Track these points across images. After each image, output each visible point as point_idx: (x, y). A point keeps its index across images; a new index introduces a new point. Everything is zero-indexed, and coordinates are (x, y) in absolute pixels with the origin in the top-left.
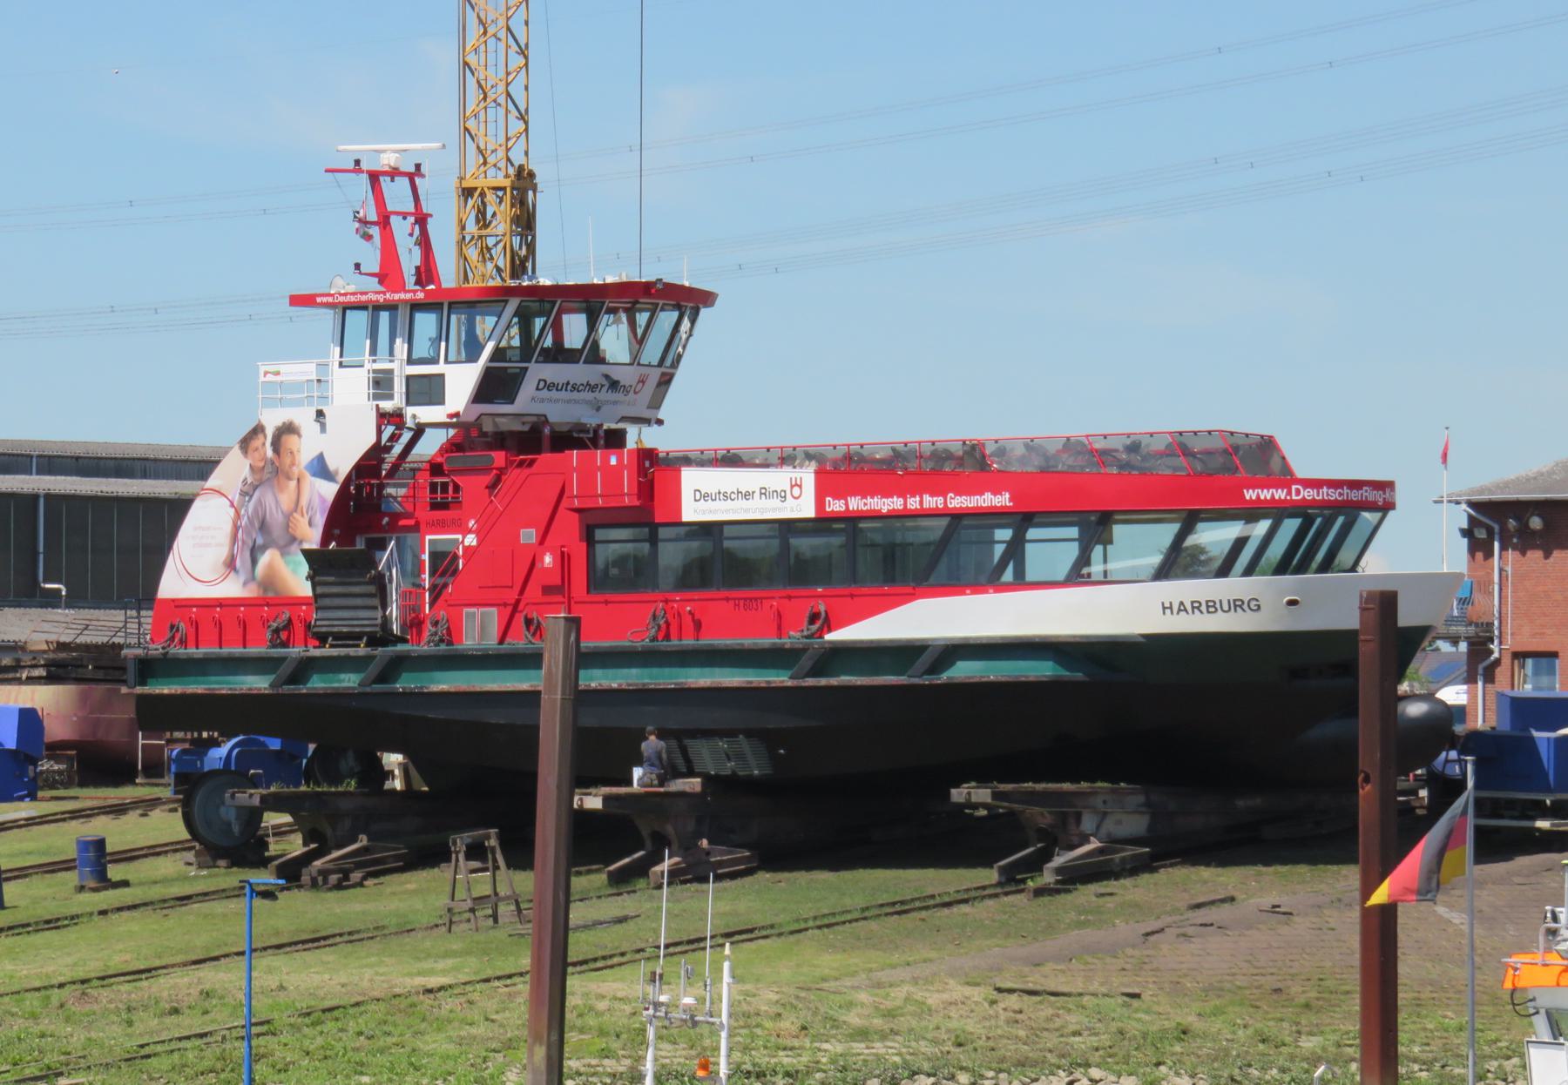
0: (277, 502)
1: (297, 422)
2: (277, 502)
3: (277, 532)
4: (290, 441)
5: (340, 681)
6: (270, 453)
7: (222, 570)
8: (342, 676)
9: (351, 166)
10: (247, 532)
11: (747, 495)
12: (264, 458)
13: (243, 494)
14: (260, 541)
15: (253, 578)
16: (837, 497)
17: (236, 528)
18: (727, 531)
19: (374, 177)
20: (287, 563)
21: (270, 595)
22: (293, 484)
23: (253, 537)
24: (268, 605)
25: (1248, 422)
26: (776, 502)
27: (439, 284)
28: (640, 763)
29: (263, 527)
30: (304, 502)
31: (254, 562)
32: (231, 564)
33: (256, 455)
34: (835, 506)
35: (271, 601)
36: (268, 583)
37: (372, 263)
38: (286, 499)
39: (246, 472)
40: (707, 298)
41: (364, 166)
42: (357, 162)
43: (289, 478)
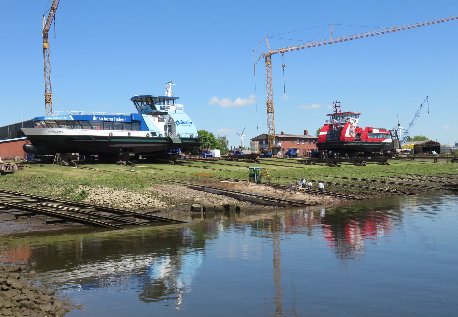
23: (351, 132)
36: (352, 136)
40: (360, 114)
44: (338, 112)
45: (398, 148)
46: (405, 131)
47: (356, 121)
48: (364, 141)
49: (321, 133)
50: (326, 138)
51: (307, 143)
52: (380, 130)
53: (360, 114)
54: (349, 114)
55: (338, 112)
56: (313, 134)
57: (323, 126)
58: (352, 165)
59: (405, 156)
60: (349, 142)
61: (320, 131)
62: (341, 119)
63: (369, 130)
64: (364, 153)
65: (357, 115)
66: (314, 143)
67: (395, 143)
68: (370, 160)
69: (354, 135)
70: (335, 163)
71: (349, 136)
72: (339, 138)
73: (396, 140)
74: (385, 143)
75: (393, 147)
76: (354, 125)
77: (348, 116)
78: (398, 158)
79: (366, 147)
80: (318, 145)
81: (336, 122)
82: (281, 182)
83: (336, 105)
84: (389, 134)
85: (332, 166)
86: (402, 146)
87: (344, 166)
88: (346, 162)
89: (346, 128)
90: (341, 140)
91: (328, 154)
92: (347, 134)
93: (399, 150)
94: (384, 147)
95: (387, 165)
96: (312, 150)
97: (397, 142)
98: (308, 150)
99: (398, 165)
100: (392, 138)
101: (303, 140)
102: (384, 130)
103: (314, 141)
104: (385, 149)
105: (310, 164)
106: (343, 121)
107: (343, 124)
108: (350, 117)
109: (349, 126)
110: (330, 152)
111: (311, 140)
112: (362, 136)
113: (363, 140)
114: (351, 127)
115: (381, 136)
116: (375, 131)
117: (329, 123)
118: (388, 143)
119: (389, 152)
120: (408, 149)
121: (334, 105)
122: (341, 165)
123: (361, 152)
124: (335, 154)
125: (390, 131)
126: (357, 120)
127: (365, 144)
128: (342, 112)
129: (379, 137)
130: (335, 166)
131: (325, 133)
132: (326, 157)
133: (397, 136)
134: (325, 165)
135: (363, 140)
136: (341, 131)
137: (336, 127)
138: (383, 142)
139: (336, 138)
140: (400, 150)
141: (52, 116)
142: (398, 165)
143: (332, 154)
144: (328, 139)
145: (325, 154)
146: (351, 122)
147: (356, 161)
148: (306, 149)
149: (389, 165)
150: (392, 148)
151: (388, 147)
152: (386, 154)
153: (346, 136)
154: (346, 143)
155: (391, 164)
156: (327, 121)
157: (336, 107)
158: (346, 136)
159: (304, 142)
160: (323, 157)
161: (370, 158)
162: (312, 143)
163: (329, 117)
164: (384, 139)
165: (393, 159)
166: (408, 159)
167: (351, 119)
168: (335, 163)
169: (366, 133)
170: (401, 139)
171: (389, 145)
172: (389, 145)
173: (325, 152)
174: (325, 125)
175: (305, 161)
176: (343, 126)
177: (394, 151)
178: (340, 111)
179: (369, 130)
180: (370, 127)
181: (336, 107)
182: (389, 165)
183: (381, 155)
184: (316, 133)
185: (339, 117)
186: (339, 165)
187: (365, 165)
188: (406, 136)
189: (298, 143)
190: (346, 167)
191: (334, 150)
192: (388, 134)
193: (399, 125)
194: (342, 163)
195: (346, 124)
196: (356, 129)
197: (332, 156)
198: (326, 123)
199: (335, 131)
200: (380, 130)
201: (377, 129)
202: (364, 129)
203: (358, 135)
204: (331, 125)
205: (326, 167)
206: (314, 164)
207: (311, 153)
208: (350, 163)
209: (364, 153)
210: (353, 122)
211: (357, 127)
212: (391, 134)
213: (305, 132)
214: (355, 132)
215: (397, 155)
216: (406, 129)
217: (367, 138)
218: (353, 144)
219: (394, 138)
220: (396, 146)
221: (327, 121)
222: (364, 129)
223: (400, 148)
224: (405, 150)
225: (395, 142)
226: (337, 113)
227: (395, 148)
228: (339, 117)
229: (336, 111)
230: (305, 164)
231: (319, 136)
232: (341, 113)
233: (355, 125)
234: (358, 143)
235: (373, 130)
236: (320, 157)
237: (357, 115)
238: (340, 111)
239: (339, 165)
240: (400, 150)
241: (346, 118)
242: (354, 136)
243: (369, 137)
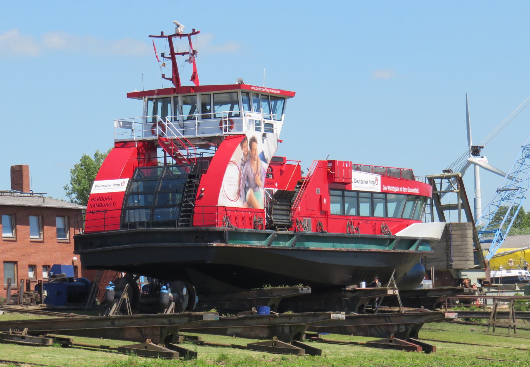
0: (251, 169)
1: (256, 137)
2: (251, 169)
3: (252, 182)
4: (254, 144)
5: (280, 244)
6: (249, 149)
7: (236, 195)
8: (280, 242)
9: (160, 35)
10: (243, 181)
11: (114, 185)
12: (247, 151)
13: (242, 165)
14: (247, 185)
15: (245, 200)
16: (386, 186)
17: (240, 179)
18: (361, 194)
19: (170, 38)
20: (255, 195)
21: (251, 208)
22: (256, 162)
23: (247, 184)
24: (237, 211)
25: (406, 166)
26: (372, 186)
27: (198, 82)
28: (386, 291)
29: (248, 179)
30: (259, 170)
31: (246, 194)
32: (239, 193)
33: (245, 149)
34: (385, 189)
35: (251, 209)
36: (250, 203)
37: (169, 74)
38: (254, 168)
39: (242, 156)
40: (291, 95)
41: (165, 34)
42: (162, 33)
43: (255, 160)
44: (185, 81)
45: (471, 264)
46: (503, 183)
47: (269, 128)
48: (309, 231)
49: (101, 187)
50: (126, 209)
51: (29, 233)
52: (388, 176)
53: (291, 95)
54: (237, 94)
55: (185, 81)
56: (52, 188)
57: (106, 147)
58: (251, 347)
59: (504, 307)
60: (236, 235)
61: (87, 172)
62: (198, 115)
63: (334, 176)
64: (308, 290)
65: (276, 99)
66: (61, 233)
67: (455, 241)
68: (339, 328)
69: (260, 199)
70: (169, 340)
71: (239, 204)
72: (188, 213)
73: (460, 226)
74: (411, 241)
75: (449, 259)
76: (260, 147)
77: (233, 103)
78: (467, 319)
79: (309, 258)
80: (81, 244)
81: (173, 132)
82: (505, 330)
83: (174, 45)
84: (429, 197)
85: (153, 354)
86: (487, 256)
87: (215, 352)
88: (223, 332)
89: (224, 161)
90: (199, 222)
91: (134, 288)
92: (229, 196)
93: (473, 277)
94: (396, 260)
95: (420, 354)
96: (57, 268)
97: (464, 236)
98: (32, 267)
99: (474, 350)
100: (442, 218)
101: (6, 219)
102: (404, 177)
103: (60, 222)
104: (408, 269)
105: (44, 344)
106: (210, 128)
107: (208, 142)
108: (244, 110)
109: (238, 154)
110: (143, 280)
111: (45, 215)
112: (298, 206)
113: (307, 225)
114: (249, 157)
115: (392, 207)
116: (364, 182)
117: (138, 134)
118: (425, 242)
119: (427, 284)
120: (515, 273)
121: (163, 45)
122: (199, 349)
123: (293, 282)
124: (167, 293)
125: (431, 180)
126: (278, 126)
127: (313, 246)
128: (203, 82)
129: (379, 212)
130: (168, 356)
131: (118, 186)
132: (122, 309)
133: (465, 205)
134: (122, 350)
135: (307, 225)
136: (200, 175)
137: (175, 157)
138: (402, 233)
139: (171, 213)
140: (482, 275)
141: (193, 226)
142: (474, 350)
143: (154, 290)
144: (134, 216)
145: (119, 290)
146: (250, 132)
147: (273, 330)
148: (23, 264)
149: (428, 349)
150: (442, 265)
151: (425, 259)
152: (413, 297)
153: (222, 201)
154: (220, 236)
155: (439, 346)
156: (127, 125)
157: (173, 55)
158: (222, 201)
159: (13, 227)
160: (107, 304)
161: (342, 316)
162: (50, 231)
163: (140, 103)
164: (404, 223)
165: (450, 321)
166: (519, 322)
167: (249, 120)
168: (169, 340)
169: (318, 191)
170: (482, 221)
171: (427, 249)
172: (427, 249)
173: (117, 282)
174: (121, 145)
175: (18, 325)
176: (210, 153)
177: (451, 283)
178: (194, 78)
179: (334, 176)
180: (337, 158)
181: (173, 55)
182: (428, 349)
183: (391, 301)
184: (67, 179)
185: (187, 109)
186: (190, 347)
187: (315, 352)
188: (509, 204)
189: (8, 235)
190: (223, 358)
191: (161, 272)
192: (425, 199)
193: (476, 151)
194: (204, 337)
195: (225, 144)
196: (271, 171)
197: (150, 303)
198: (126, 135)
199: (170, 178)
200: (388, 176)
201: (372, 170)
202: (308, 169)
203: (283, 199)
204: (148, 147)
205: (124, 358)
206: (66, 344)
207: (47, 286)
208: (244, 342)
209: (308, 290)
210: (258, 135)
211: (277, 163)
212: (437, 197)
213: (18, 176)
214: (268, 184)
215: (466, 302)
216: (509, 171)
217: (324, 211)
218: (256, 244)
219: (452, 217)
220: (463, 256)
221: (127, 125)
222: (308, 169)
223: (481, 263)
224: (504, 273)
225: (455, 234)
226: (178, 89)
227: (456, 264)
228: (187, 109)
229: (176, 79)
230: (21, 342)
231: (84, 194)
232: (198, 89)
233: (267, 147)
234: (281, 237)
235: (356, 175)
236: (94, 309)
237: (275, 98)
238: (194, 78)
239: (190, 347)
240: (482, 275)
241: (222, 111)
242: (260, 203)
243: (335, 209)
